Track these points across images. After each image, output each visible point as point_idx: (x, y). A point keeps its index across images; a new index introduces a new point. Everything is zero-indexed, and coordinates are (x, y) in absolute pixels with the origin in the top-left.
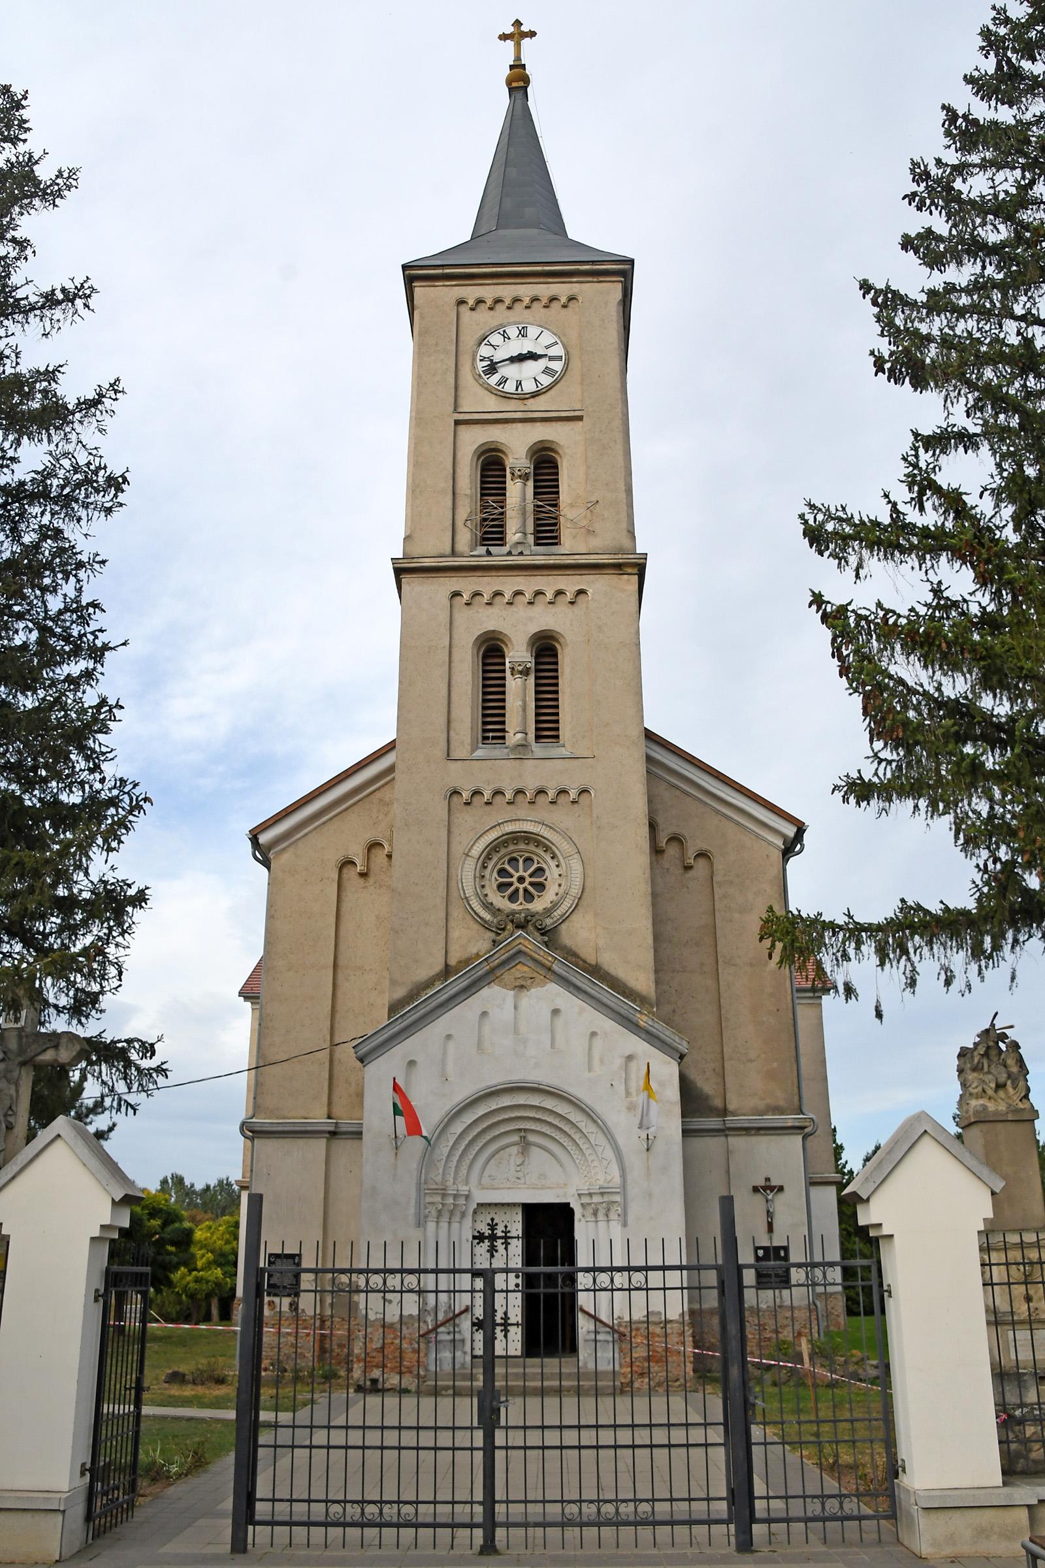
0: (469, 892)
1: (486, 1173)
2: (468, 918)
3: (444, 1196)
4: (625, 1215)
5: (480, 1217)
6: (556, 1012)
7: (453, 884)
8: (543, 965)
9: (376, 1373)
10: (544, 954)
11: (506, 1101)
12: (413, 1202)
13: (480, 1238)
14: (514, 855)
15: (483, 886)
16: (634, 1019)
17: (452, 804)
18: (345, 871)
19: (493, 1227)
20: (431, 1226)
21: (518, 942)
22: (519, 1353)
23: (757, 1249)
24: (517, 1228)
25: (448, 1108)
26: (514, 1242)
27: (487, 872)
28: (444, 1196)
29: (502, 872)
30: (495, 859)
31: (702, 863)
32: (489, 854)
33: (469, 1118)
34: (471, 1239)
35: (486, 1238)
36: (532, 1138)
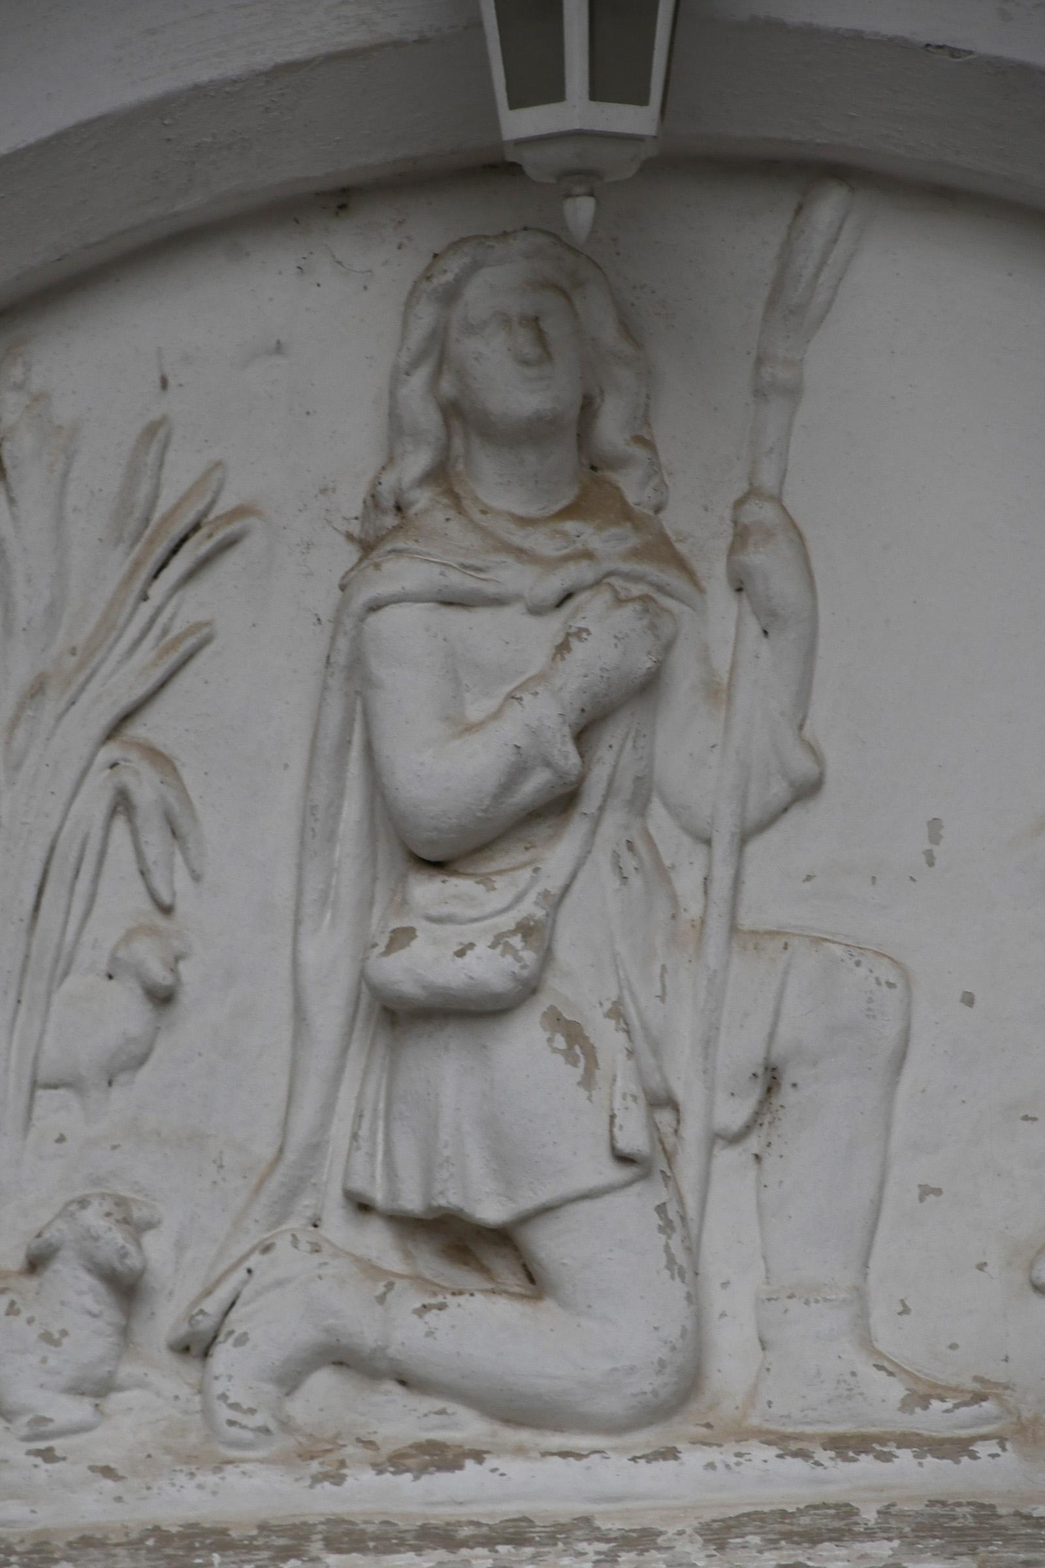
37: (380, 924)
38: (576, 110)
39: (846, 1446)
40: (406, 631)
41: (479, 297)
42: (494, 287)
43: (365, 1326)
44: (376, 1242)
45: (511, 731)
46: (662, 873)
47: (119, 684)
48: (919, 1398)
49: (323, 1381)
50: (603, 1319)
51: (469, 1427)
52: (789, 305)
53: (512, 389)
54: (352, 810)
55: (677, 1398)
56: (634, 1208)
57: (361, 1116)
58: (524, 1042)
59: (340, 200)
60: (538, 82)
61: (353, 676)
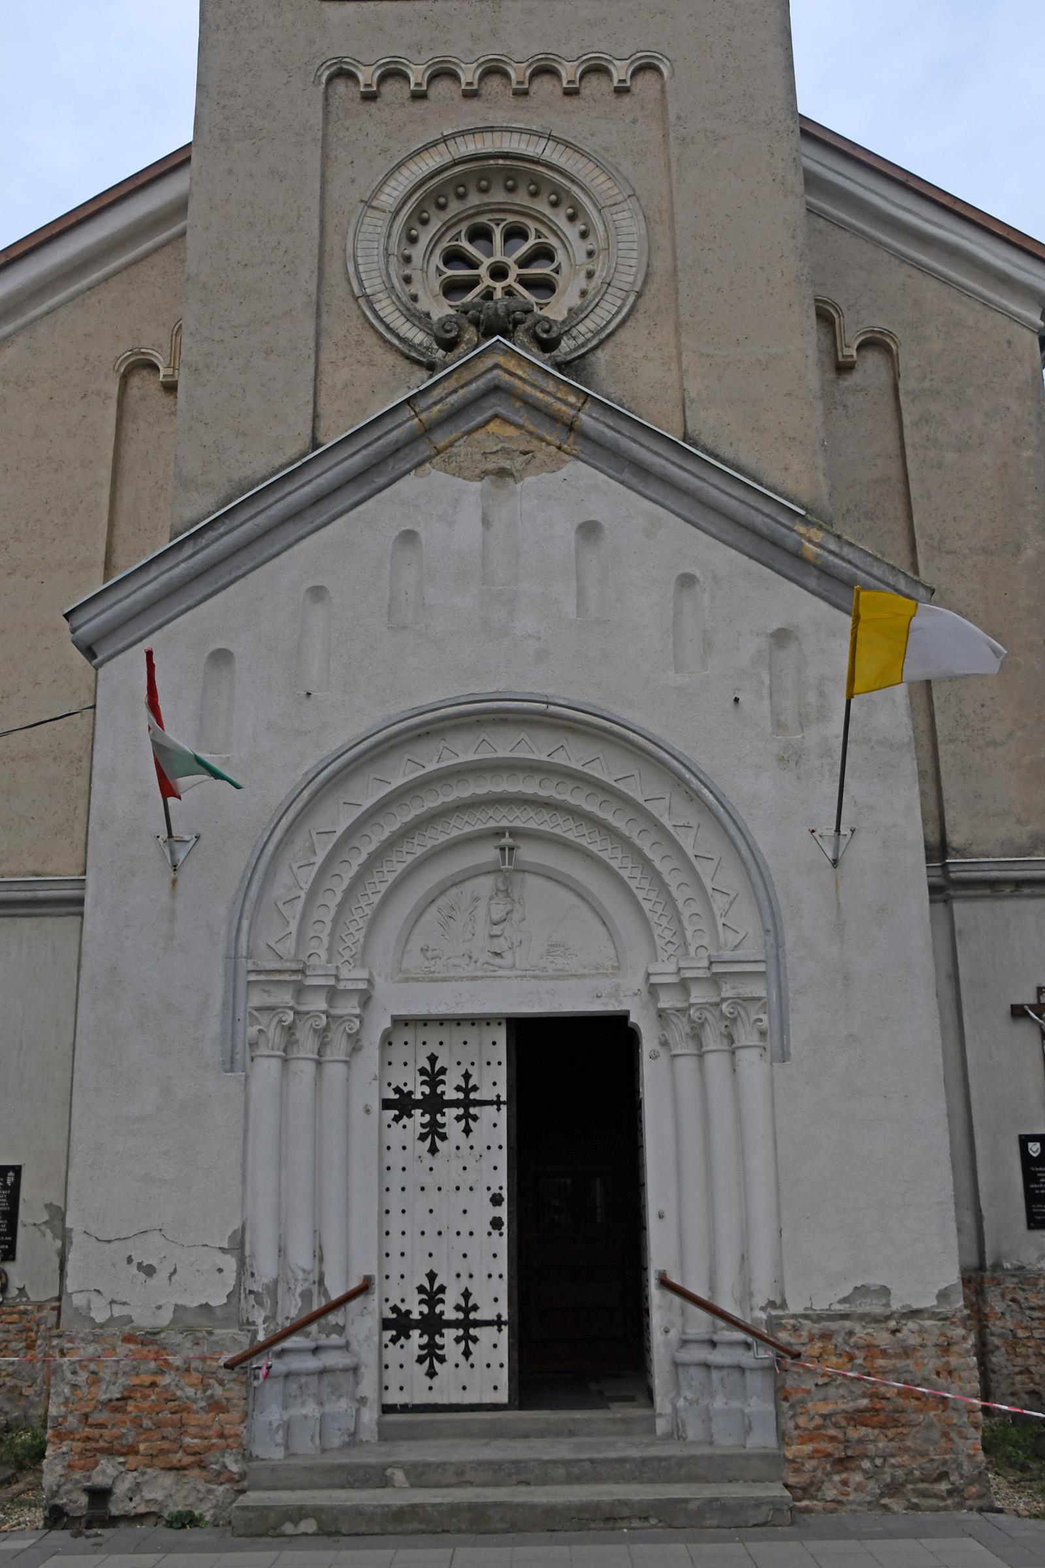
0: (373, 284)
2: (370, 339)
3: (300, 990)
4: (783, 1029)
5: (399, 1053)
6: (589, 530)
7: (334, 268)
8: (553, 418)
9: (105, 1472)
10: (552, 394)
11: (464, 750)
13: (402, 1104)
14: (483, 219)
15: (408, 280)
16: (791, 540)
17: (335, 102)
18: (135, 381)
19: (433, 1077)
20: (267, 1070)
21: (489, 362)
22: (503, 1397)
23: (1024, 1140)
24: (494, 1081)
26: (487, 1114)
27: (417, 252)
28: (300, 990)
29: (454, 257)
30: (435, 225)
31: (873, 362)
32: (419, 209)
33: (368, 792)
34: (376, 1105)
35: (417, 1104)
36: (528, 853)
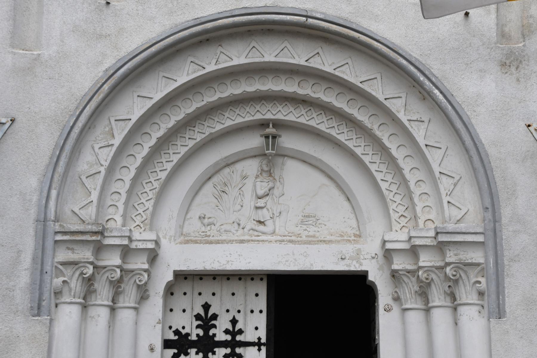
1: (195, 212)
5: (179, 302)
12: (27, 259)
19: (206, 321)
25: (109, 62)
28: (99, 248)
33: (157, 88)
34: (159, 345)
35: (193, 344)
37: (256, 202)
38: (270, 151)
39: (284, 236)
40: (258, 184)
41: (264, 163)
42: (265, 162)
43: (254, 227)
44: (255, 222)
45: (265, 190)
46: (274, 199)
47: (240, 186)
48: (289, 233)
49: (251, 231)
50: (269, 228)
51: (260, 234)
52: (283, 164)
53: (266, 169)
54: (254, 195)
55: (274, 233)
56: (271, 220)
57: (269, 30)
58: (265, 210)
59: (255, 156)
60: (268, 149)
61: (255, 186)
